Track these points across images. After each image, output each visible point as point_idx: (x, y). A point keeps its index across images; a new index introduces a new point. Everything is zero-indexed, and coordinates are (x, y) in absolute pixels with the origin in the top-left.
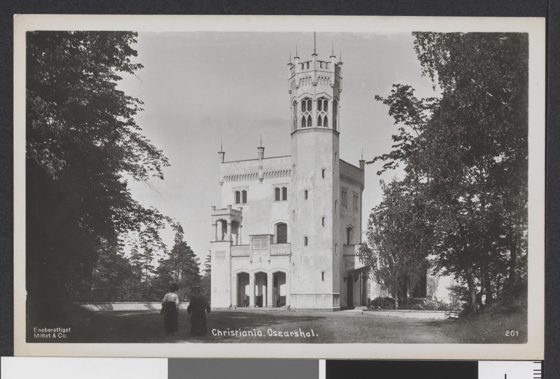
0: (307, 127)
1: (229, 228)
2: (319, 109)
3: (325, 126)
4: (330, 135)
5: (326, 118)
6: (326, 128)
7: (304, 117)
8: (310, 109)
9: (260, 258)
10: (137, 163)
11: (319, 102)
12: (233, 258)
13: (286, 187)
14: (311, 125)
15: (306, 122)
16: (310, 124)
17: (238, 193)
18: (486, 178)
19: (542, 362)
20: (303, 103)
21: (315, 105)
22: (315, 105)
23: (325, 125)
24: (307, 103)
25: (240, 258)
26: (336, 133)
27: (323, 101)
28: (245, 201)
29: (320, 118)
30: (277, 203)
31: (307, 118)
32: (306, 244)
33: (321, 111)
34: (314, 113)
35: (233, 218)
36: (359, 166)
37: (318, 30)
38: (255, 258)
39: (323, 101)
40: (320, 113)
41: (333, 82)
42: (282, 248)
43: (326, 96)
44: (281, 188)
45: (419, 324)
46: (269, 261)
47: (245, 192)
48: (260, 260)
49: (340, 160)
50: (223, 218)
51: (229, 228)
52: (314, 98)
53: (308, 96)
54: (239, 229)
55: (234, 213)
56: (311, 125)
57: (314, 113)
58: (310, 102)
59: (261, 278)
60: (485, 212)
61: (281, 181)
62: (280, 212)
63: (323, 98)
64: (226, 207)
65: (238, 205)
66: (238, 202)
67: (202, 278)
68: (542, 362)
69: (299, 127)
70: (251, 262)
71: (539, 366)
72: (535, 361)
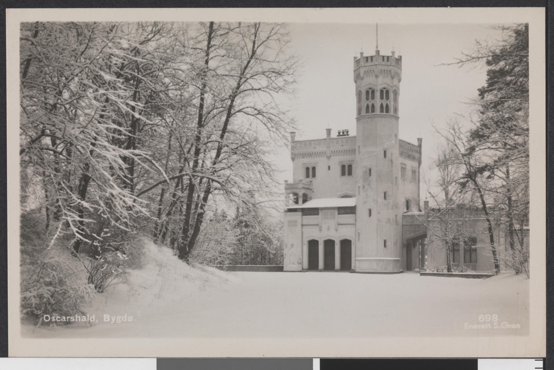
0: (384, 113)
2: (382, 98)
5: (373, 106)
8: (373, 98)
9: (328, 227)
10: (430, 154)
11: (382, 91)
12: (304, 227)
17: (308, 169)
19: (544, 360)
20: (367, 92)
21: (378, 95)
22: (378, 95)
24: (370, 93)
25: (310, 227)
27: (385, 91)
28: (314, 176)
29: (382, 106)
30: (344, 178)
31: (385, 106)
32: (370, 215)
34: (378, 102)
37: (216, 20)
38: (324, 227)
39: (385, 91)
40: (368, 102)
47: (314, 168)
48: (329, 229)
49: (400, 140)
52: (379, 88)
53: (371, 86)
58: (373, 92)
59: (329, 243)
63: (384, 88)
65: (308, 180)
66: (308, 176)
68: (544, 360)
71: (540, 364)
72: (537, 359)
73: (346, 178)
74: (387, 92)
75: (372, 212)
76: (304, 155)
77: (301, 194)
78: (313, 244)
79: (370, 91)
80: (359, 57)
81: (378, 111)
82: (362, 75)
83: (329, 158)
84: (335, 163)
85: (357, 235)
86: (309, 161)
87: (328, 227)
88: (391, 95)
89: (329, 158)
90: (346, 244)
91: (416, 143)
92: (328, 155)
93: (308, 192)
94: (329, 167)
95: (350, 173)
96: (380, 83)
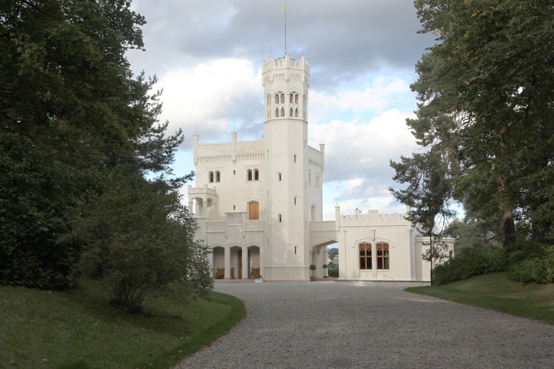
0: (280, 118)
1: (205, 205)
2: (291, 101)
3: (296, 116)
4: (301, 124)
5: (283, 109)
6: (291, 118)
7: (277, 108)
14: (284, 116)
15: (280, 113)
16: (283, 115)
21: (287, 98)
22: (287, 98)
23: (296, 116)
24: (279, 97)
26: (306, 123)
27: (294, 95)
34: (287, 105)
35: (209, 197)
36: (319, 150)
39: (294, 95)
40: (292, 105)
41: (303, 79)
42: (254, 225)
50: (200, 196)
54: (537, 321)
55: (210, 192)
57: (287, 105)
59: (237, 251)
61: (253, 164)
64: (202, 187)
69: (273, 117)
70: (226, 237)
73: (253, 182)
82: (271, 79)
87: (283, 108)
88: (300, 98)
90: (254, 251)
92: (234, 159)
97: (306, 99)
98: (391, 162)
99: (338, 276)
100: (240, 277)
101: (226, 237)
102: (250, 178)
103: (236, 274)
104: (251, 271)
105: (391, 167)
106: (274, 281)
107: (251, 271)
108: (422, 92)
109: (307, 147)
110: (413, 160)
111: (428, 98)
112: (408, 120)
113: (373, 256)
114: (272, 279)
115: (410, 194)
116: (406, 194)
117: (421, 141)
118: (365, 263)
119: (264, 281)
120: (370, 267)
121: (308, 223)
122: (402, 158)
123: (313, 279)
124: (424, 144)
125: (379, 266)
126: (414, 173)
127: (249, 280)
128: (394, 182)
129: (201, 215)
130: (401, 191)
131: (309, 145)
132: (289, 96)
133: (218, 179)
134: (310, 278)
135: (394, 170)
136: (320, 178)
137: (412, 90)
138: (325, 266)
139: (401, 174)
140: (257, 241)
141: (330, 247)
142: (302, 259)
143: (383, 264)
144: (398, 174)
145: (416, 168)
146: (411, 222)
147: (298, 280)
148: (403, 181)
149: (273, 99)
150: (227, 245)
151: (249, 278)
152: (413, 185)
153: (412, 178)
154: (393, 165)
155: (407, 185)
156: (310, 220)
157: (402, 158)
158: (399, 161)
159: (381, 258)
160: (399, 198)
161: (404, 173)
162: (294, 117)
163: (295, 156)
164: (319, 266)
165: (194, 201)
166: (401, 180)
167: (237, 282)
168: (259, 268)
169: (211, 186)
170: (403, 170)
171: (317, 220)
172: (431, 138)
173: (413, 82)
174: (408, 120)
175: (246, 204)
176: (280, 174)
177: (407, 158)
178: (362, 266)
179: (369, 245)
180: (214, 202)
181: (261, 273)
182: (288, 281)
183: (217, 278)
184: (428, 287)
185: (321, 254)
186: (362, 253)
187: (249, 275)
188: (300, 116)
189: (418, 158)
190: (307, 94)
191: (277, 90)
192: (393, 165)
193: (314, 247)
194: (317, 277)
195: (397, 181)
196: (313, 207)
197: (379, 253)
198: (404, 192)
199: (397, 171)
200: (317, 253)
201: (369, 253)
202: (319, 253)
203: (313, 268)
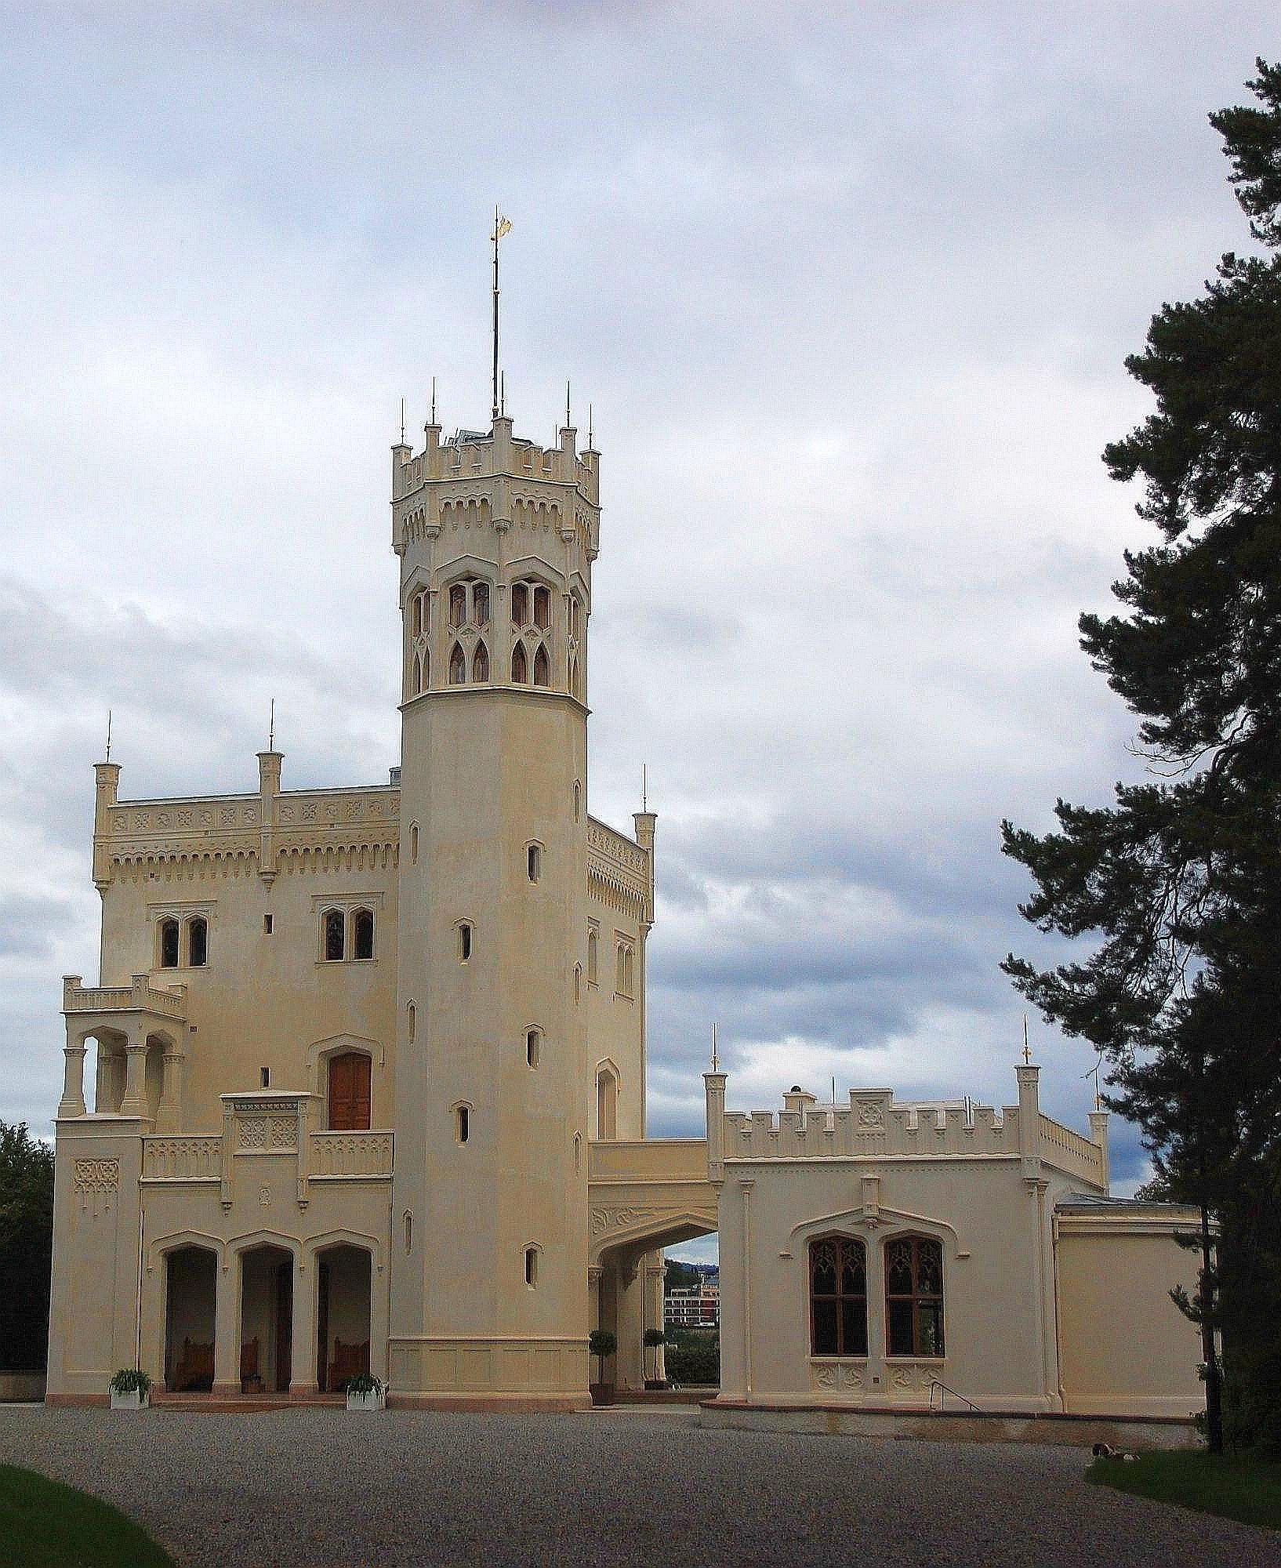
1: (137, 1064)
2: (518, 616)
5: (481, 651)
6: (540, 689)
11: (519, 591)
13: (369, 907)
18: (1229, 864)
21: (501, 605)
22: (501, 605)
24: (469, 591)
27: (532, 588)
29: (519, 652)
30: (334, 968)
31: (469, 648)
33: (525, 628)
35: (153, 1027)
39: (532, 588)
42: (349, 1155)
43: (544, 572)
44: (347, 910)
45: (1076, 1144)
46: (303, 1205)
49: (590, 818)
50: (118, 1024)
51: (137, 1064)
56: (484, 679)
59: (268, 1269)
60: (1254, 672)
61: (345, 886)
62: (347, 1004)
67: (1237, 159)
70: (226, 1206)
73: (351, 971)
74: (542, 594)
75: (540, 1260)
76: (148, 865)
77: (137, 1039)
78: (189, 1269)
79: (468, 588)
80: (418, 444)
81: (501, 673)
82: (432, 521)
83: (269, 879)
84: (303, 899)
85: (400, 1226)
86: (180, 897)
87: (481, 644)
88: (557, 607)
89: (269, 879)
90: (346, 1269)
91: (624, 826)
92: (267, 868)
93: (174, 1032)
94: (269, 919)
95: (364, 949)
96: (509, 560)
97: (584, 610)
98: (1008, 833)
99: (715, 1381)
100: (283, 1382)
101: (226, 1206)
102: (334, 950)
103: (266, 1368)
104: (331, 1359)
105: (1011, 860)
106: (430, 1405)
107: (331, 1359)
108: (1167, 477)
109: (583, 819)
110: (1124, 818)
111: (1205, 505)
112: (1088, 623)
113: (875, 1289)
114: (425, 1395)
115: (1112, 990)
116: (1090, 988)
117: (1161, 722)
118: (836, 1329)
119: (389, 1404)
120: (857, 1345)
121: (584, 1147)
122: (1063, 811)
123: (604, 1393)
124: (1179, 738)
125: (901, 1341)
126: (1130, 883)
127: (322, 1398)
128: (1030, 929)
129: (117, 1109)
130: (1062, 971)
131: (592, 811)
132: (508, 595)
133: (198, 956)
134: (592, 1388)
135: (1026, 870)
136: (636, 958)
137: (1116, 476)
138: (652, 1339)
139: (1063, 891)
140: (353, 1220)
141: (682, 1253)
142: (563, 1310)
143: (916, 1330)
144: (1048, 889)
145: (1150, 855)
146: (1137, 1126)
147: (537, 1402)
148: (1076, 924)
149: (440, 607)
150: (227, 1239)
151: (322, 1388)
152: (1127, 940)
153: (1123, 907)
154: (1018, 845)
155: (1088, 947)
156: (592, 1135)
157: (1063, 811)
158: (1048, 827)
159: (847, 1288)
160: (1053, 1008)
161: (1076, 885)
162: (529, 686)
163: (532, 851)
164: (629, 1336)
165: (92, 1045)
166: (1066, 919)
167: (271, 1408)
168: (367, 1345)
169: (166, 980)
170: (1079, 865)
171: (624, 1132)
172: (1216, 707)
173: (1120, 433)
174: (1088, 623)
175: (314, 1060)
176: (466, 931)
177: (1090, 810)
178: (823, 1342)
179: (855, 1247)
180: (176, 1050)
181: (376, 1368)
182: (492, 1405)
183: (183, 1389)
184: (1183, 1456)
185: (637, 1283)
186: (820, 1282)
187: (321, 1378)
188: (559, 686)
189: (1144, 807)
190: (588, 592)
191: (458, 570)
192: (1018, 845)
193: (607, 1256)
194: (620, 1384)
195: (1042, 922)
196: (605, 1080)
197: (897, 1282)
198: (1078, 976)
199: (1040, 873)
200: (619, 1283)
201: (857, 1282)
202: (628, 1277)
203: (603, 1344)
